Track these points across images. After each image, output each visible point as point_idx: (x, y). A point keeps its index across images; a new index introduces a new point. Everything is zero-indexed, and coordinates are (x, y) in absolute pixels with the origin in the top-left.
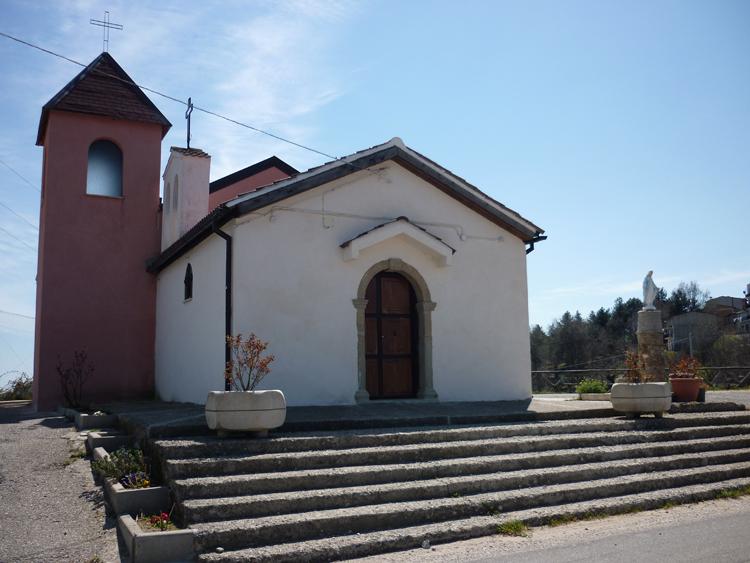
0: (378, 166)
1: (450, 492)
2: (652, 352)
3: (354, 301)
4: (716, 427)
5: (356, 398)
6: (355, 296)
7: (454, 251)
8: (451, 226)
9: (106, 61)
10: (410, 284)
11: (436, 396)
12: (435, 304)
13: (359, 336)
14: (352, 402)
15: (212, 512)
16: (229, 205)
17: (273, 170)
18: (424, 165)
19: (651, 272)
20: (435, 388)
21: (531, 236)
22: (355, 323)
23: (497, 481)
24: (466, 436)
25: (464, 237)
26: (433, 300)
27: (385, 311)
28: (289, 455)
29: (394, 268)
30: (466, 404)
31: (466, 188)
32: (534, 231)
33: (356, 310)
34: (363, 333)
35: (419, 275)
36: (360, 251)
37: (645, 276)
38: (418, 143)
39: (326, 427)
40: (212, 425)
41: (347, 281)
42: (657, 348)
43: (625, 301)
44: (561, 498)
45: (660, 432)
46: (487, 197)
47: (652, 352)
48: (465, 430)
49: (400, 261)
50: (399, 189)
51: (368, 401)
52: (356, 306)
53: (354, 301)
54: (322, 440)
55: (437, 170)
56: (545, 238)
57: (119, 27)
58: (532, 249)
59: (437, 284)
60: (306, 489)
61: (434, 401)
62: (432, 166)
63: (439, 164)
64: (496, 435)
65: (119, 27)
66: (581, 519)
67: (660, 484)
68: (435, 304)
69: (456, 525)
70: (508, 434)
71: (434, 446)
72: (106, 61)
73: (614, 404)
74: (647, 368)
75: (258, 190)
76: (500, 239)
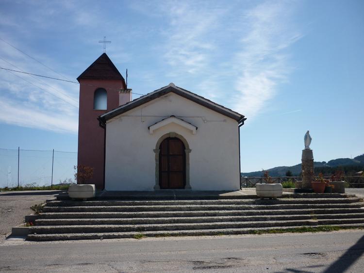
0: (165, 95)
2: (306, 169)
3: (154, 150)
5: (154, 188)
6: (155, 148)
7: (197, 128)
8: (201, 117)
9: (104, 57)
10: (182, 142)
11: (191, 188)
12: (191, 150)
13: (156, 164)
14: (153, 190)
15: (42, 223)
16: (101, 117)
17: (173, 97)
18: (184, 93)
19: (308, 132)
20: (190, 184)
21: (241, 119)
22: (155, 158)
24: (165, 203)
25: (205, 121)
26: (190, 148)
27: (171, 154)
28: (83, 207)
30: (143, 192)
31: (204, 100)
32: (240, 116)
34: (158, 163)
35: (184, 138)
36: (153, 131)
37: (305, 133)
38: (180, 84)
39: (129, 199)
40: (71, 196)
41: (151, 142)
42: (308, 167)
45: (263, 206)
46: (214, 103)
47: (306, 169)
48: (170, 201)
50: (174, 103)
51: (159, 189)
52: (155, 152)
53: (154, 150)
54: (102, 203)
55: (191, 95)
56: (246, 119)
58: (243, 124)
59: (191, 141)
60: (162, 223)
61: (189, 190)
62: (188, 93)
63: (192, 92)
64: (178, 204)
65: (110, 42)
66: (173, 236)
67: (229, 226)
68: (191, 150)
69: (116, 234)
70: (185, 204)
71: (140, 206)
72: (104, 57)
73: (257, 193)
74: (304, 177)
75: (113, 110)
76: (225, 121)
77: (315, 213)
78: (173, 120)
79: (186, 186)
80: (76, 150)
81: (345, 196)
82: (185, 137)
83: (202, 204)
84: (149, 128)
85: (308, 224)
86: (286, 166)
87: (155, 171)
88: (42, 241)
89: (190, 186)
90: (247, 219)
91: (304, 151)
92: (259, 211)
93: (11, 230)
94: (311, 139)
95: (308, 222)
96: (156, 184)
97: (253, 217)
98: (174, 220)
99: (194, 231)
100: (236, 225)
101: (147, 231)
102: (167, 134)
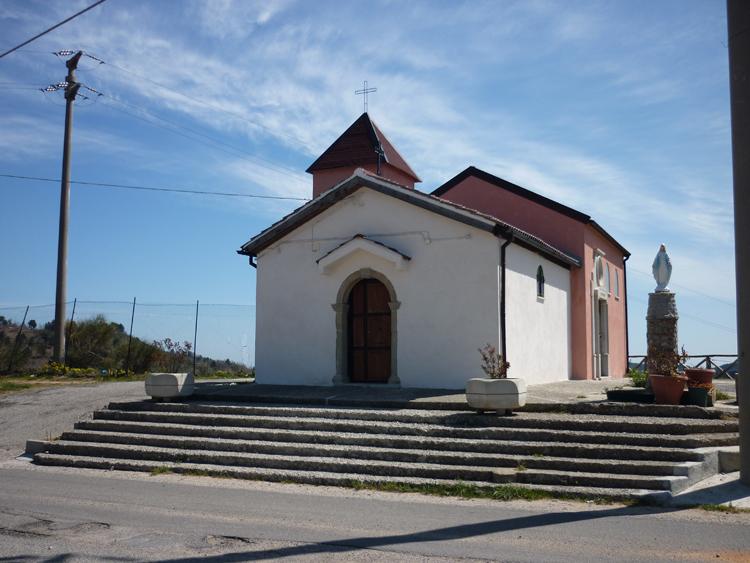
1: (241, 449)
3: (333, 306)
4: (600, 434)
5: (333, 381)
6: (334, 302)
8: (420, 233)
9: (365, 118)
11: (399, 382)
14: (331, 384)
17: (472, 179)
20: (398, 375)
23: (216, 444)
26: (399, 299)
27: (370, 311)
29: (367, 276)
33: (335, 313)
43: (13, 322)
44: (233, 461)
49: (371, 270)
53: (333, 306)
57: (374, 90)
59: (405, 284)
65: (374, 90)
67: (325, 467)
70: (308, 415)
72: (365, 118)
76: (469, 236)
77: (440, 463)
78: (359, 243)
79: (392, 379)
80: (254, 303)
81: (717, 415)
82: (389, 278)
83: (338, 416)
84: (318, 262)
85: (490, 477)
86: (646, 331)
87: (335, 346)
88: (58, 465)
89: (397, 378)
90: (379, 456)
91: (652, 296)
92: (435, 440)
93: (25, 445)
94: (669, 267)
95: (491, 473)
96: (338, 373)
97: (389, 453)
98: (575, 436)
99: (247, 470)
100: (338, 465)
101: (190, 462)
102: (355, 273)
